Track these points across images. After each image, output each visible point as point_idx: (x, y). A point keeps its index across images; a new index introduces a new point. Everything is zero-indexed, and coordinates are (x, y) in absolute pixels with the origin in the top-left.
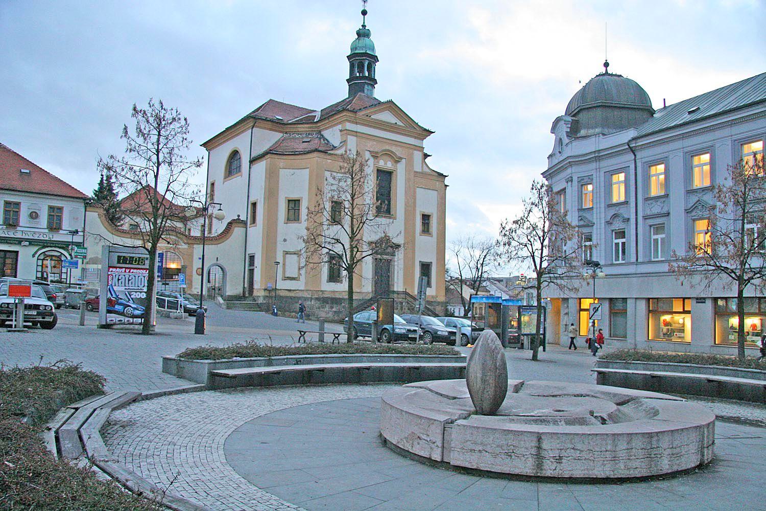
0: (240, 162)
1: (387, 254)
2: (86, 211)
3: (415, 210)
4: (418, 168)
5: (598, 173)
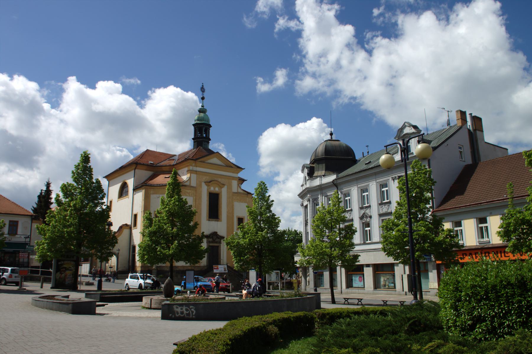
0: (128, 189)
1: (217, 243)
2: (32, 223)
3: (233, 216)
4: (235, 189)
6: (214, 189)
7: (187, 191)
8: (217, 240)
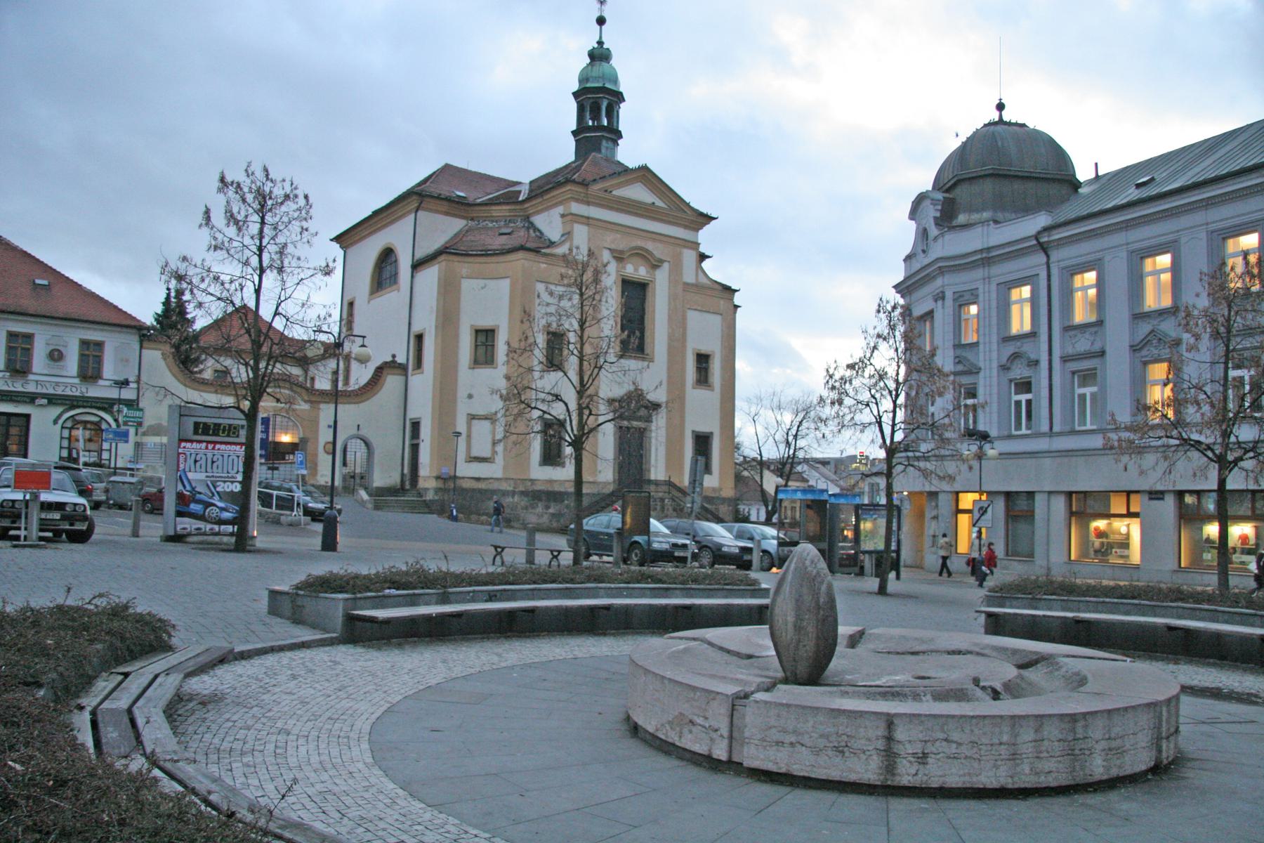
1: (639, 419)
2: (141, 347)
4: (689, 276)
6: (636, 270)
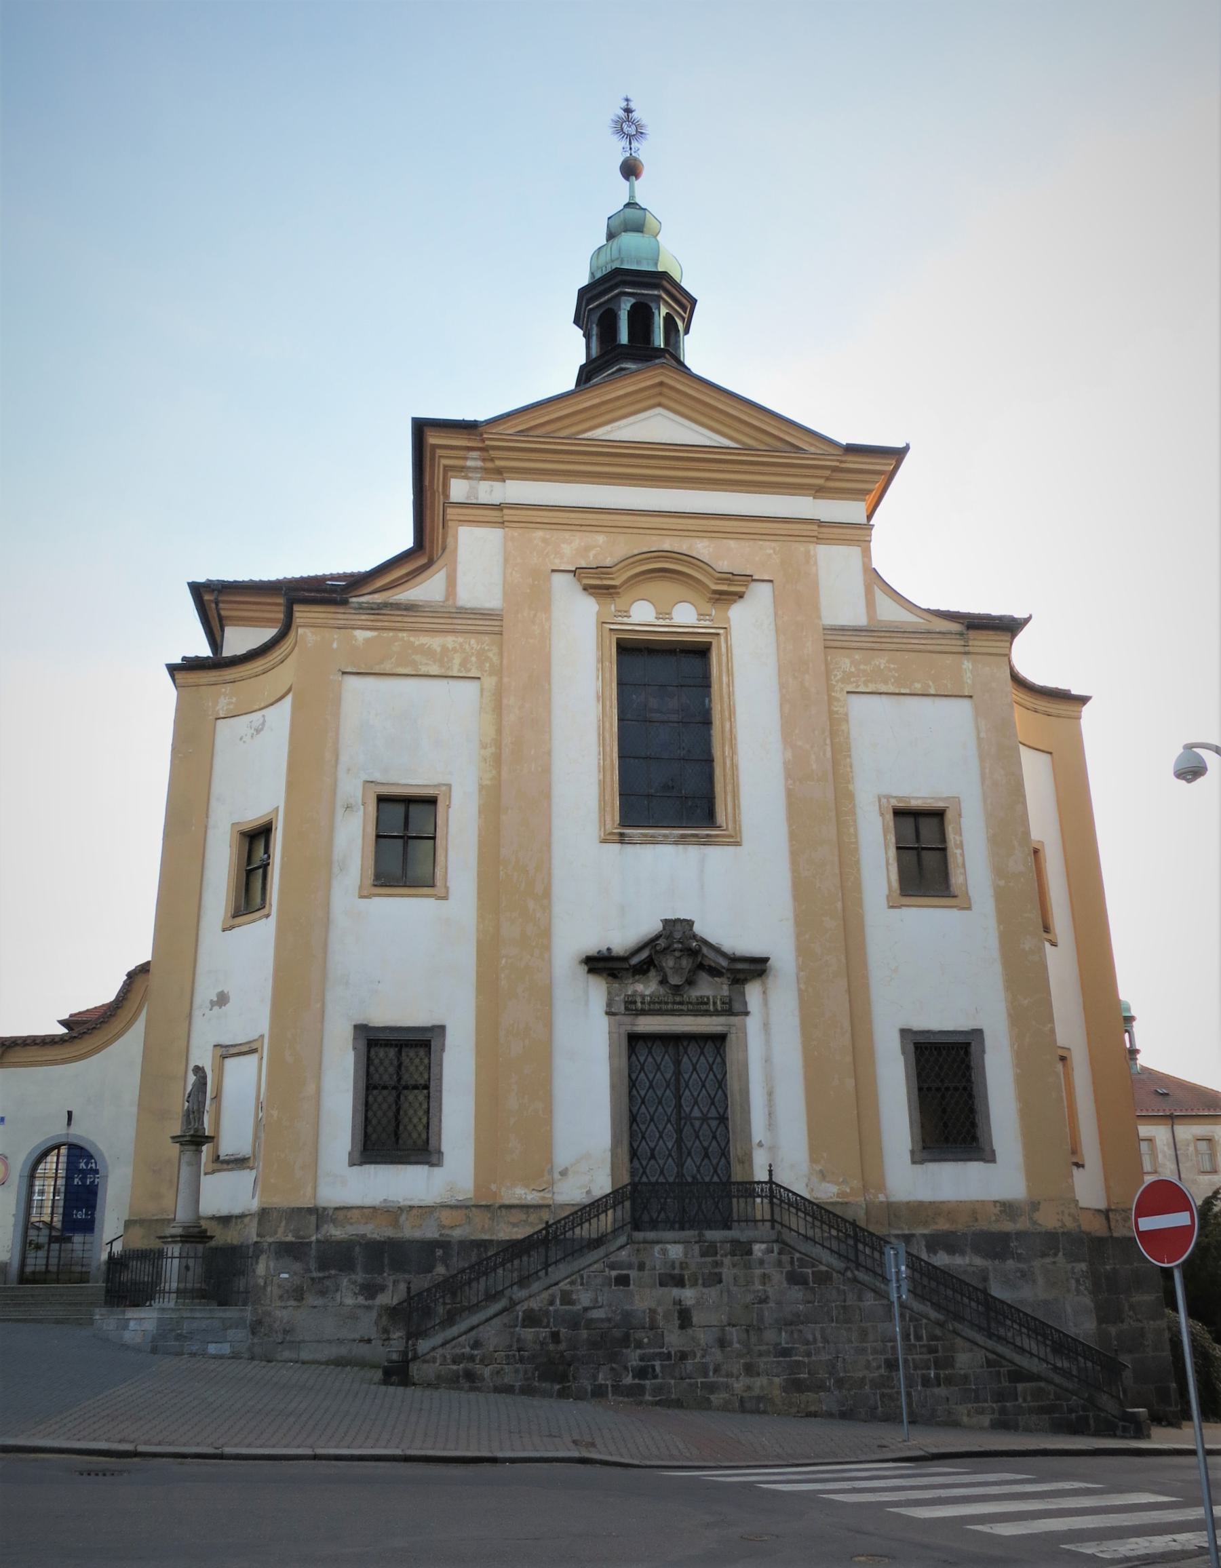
1: (701, 1008)
5: (179, 1239)
6: (664, 613)
7: (424, 640)
8: (706, 988)
